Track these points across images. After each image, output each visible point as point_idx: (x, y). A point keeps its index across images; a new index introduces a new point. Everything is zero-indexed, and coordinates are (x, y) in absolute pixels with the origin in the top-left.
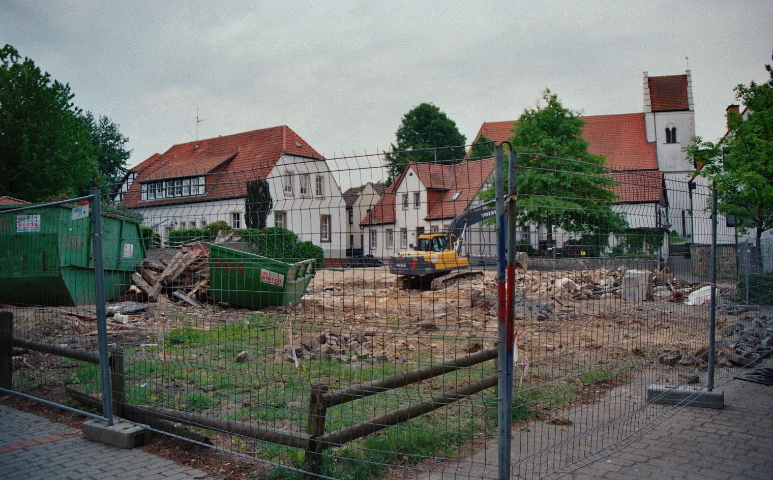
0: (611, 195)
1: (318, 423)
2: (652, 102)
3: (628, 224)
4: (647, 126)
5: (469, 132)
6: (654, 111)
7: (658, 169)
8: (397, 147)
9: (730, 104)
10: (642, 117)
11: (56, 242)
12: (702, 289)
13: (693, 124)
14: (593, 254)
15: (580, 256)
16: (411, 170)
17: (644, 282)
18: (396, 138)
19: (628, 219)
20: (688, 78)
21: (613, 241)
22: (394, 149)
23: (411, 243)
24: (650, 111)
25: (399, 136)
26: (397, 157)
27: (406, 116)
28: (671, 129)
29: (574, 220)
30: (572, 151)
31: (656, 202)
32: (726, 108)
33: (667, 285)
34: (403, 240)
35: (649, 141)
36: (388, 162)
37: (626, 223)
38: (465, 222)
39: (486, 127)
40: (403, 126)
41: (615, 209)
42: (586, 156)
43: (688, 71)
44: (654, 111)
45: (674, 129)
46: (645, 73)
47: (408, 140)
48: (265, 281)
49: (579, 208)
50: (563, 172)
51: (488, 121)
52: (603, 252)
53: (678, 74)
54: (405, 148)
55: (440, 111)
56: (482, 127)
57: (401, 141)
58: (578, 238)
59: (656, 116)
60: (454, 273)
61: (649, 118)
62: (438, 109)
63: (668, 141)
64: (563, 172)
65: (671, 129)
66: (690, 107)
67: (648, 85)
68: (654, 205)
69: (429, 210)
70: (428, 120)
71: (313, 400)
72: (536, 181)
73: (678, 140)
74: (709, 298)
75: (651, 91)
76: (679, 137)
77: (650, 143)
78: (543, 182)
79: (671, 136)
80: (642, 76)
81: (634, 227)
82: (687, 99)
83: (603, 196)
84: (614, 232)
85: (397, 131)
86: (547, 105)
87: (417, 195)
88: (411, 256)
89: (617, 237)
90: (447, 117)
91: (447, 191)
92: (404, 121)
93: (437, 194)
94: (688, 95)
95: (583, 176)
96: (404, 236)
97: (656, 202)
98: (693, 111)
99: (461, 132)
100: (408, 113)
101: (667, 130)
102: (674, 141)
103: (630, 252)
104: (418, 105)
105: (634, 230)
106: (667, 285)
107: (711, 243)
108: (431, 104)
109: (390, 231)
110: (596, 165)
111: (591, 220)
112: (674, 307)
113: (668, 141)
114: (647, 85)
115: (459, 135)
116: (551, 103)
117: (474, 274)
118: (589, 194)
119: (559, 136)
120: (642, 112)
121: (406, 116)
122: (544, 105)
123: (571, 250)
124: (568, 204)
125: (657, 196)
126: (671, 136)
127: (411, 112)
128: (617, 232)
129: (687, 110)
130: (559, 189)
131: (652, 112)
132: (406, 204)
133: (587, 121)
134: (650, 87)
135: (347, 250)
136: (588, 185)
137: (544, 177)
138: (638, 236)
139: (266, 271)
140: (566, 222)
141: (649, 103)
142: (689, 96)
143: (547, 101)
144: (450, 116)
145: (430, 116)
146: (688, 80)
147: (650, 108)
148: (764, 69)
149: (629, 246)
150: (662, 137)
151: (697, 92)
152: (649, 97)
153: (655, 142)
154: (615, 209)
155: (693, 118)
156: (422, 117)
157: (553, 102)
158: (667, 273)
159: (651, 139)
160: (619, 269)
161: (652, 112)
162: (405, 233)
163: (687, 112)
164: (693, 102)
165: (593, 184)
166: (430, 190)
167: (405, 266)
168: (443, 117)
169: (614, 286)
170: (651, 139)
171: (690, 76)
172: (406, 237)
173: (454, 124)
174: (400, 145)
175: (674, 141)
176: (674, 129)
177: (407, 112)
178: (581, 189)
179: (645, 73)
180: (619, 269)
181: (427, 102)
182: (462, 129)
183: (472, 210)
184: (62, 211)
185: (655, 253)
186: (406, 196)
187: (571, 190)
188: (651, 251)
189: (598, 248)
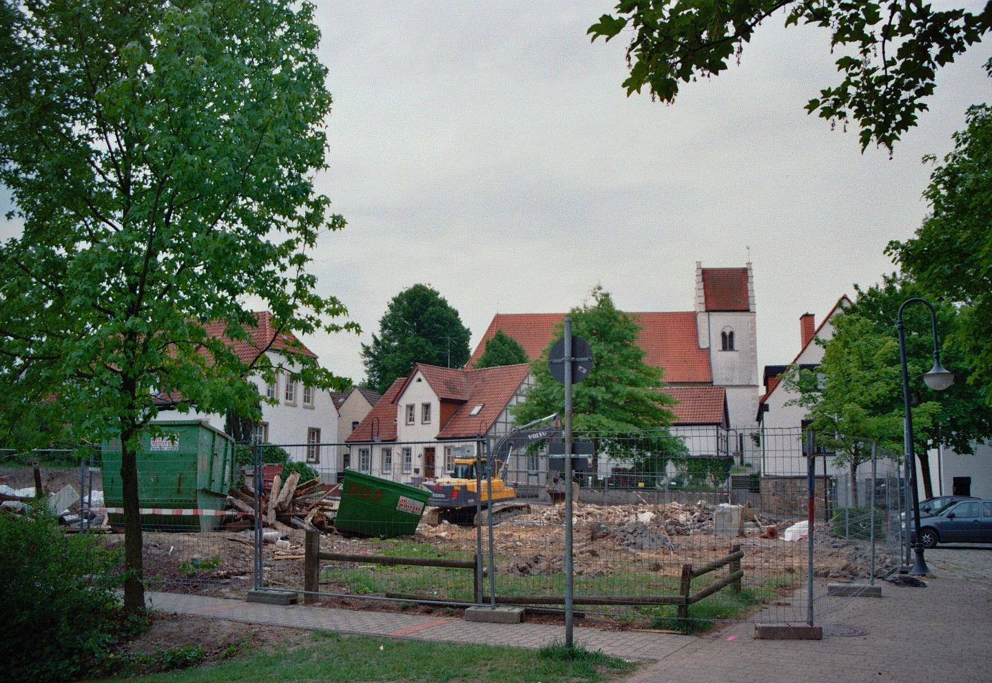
0: (669, 415)
1: (685, 587)
2: (706, 300)
3: (688, 450)
4: (700, 328)
5: (477, 325)
6: (708, 311)
7: (712, 382)
8: (380, 339)
9: (805, 313)
10: (693, 316)
11: (196, 463)
12: (797, 524)
13: (754, 328)
14: (650, 486)
15: (638, 489)
16: (419, 375)
17: (736, 519)
18: (379, 327)
19: (688, 444)
20: (749, 272)
21: (671, 469)
22: (376, 342)
23: (416, 467)
24: (704, 310)
25: (384, 324)
26: (379, 353)
27: (394, 299)
28: (728, 334)
29: (625, 443)
30: (625, 361)
31: (718, 424)
32: (800, 316)
33: (754, 521)
34: (405, 463)
35: (702, 347)
36: (367, 359)
37: (685, 449)
38: (511, 445)
39: (498, 319)
40: (389, 313)
41: (673, 432)
42: (641, 368)
43: (749, 264)
44: (708, 311)
45: (732, 334)
46: (699, 263)
47: (395, 331)
48: (402, 509)
49: (632, 429)
50: (617, 387)
51: (502, 312)
52: (659, 483)
53: (738, 267)
54: (390, 341)
55: (439, 296)
56: (494, 320)
57: (386, 332)
58: (630, 467)
59: (711, 317)
60: (498, 506)
61: (702, 319)
62: (438, 294)
63: (724, 349)
64: (617, 387)
65: (728, 334)
66: (751, 307)
67: (701, 277)
68: (715, 427)
69: (443, 425)
70: (425, 307)
71: (684, 573)
72: (583, 396)
73: (736, 347)
74: (806, 533)
75: (705, 286)
76: (736, 345)
77: (703, 349)
78: (591, 397)
79: (728, 341)
80: (695, 267)
81: (697, 454)
82: (747, 298)
83: (660, 418)
84: (673, 460)
85: (381, 319)
86: (596, 304)
87: (427, 407)
88: (452, 484)
89: (676, 465)
90: (449, 305)
91: (463, 403)
92: (391, 307)
93: (452, 406)
94: (749, 292)
95: (641, 392)
96: (407, 459)
97: (718, 424)
98: (755, 312)
99: (466, 324)
100: (398, 295)
101: (724, 334)
102: (731, 348)
103: (691, 484)
104: (411, 286)
105: (696, 459)
106: (754, 521)
107: (805, 474)
108: (428, 286)
109: (388, 452)
110: (650, 377)
111: (646, 445)
112: (771, 543)
113: (724, 349)
114: (700, 278)
115: (463, 328)
116: (601, 302)
117: (519, 508)
118: (642, 413)
119: (610, 343)
120: (693, 310)
121: (394, 299)
122: (593, 303)
123: (621, 480)
124: (623, 425)
125: (720, 419)
126: (728, 341)
127: (401, 294)
128: (677, 461)
129: (748, 311)
130: (611, 408)
131: (707, 311)
132: (411, 418)
133: (621, 318)
134: (704, 280)
135: (339, 474)
136: (643, 401)
137: (594, 392)
138: (701, 464)
139: (404, 498)
140: (611, 446)
141: (703, 300)
142: (750, 294)
143: (597, 300)
144: (451, 303)
145: (238, 245)
146: (749, 274)
147: (704, 306)
148: (853, 287)
149: (691, 477)
150: (717, 343)
151: (759, 288)
152: (702, 293)
153: (709, 349)
154: (673, 432)
155: (754, 322)
156: (417, 302)
157: (605, 301)
158: (750, 507)
159: (703, 345)
160: (699, 503)
161: (707, 311)
162: (408, 454)
163: (748, 314)
164: (754, 301)
165: (650, 402)
166: (443, 401)
167: (443, 496)
168: (443, 303)
169: (698, 521)
170: (703, 345)
171: (750, 269)
172: (409, 460)
173: (456, 314)
174: (385, 337)
175: (731, 348)
176: (732, 334)
177: (396, 295)
178: (636, 408)
179: (699, 263)
180: (699, 503)
181: (418, 283)
182: (466, 321)
183: (519, 430)
184: (200, 429)
185: (721, 485)
186: (411, 408)
187: (622, 408)
188: (716, 484)
189: (654, 479)
